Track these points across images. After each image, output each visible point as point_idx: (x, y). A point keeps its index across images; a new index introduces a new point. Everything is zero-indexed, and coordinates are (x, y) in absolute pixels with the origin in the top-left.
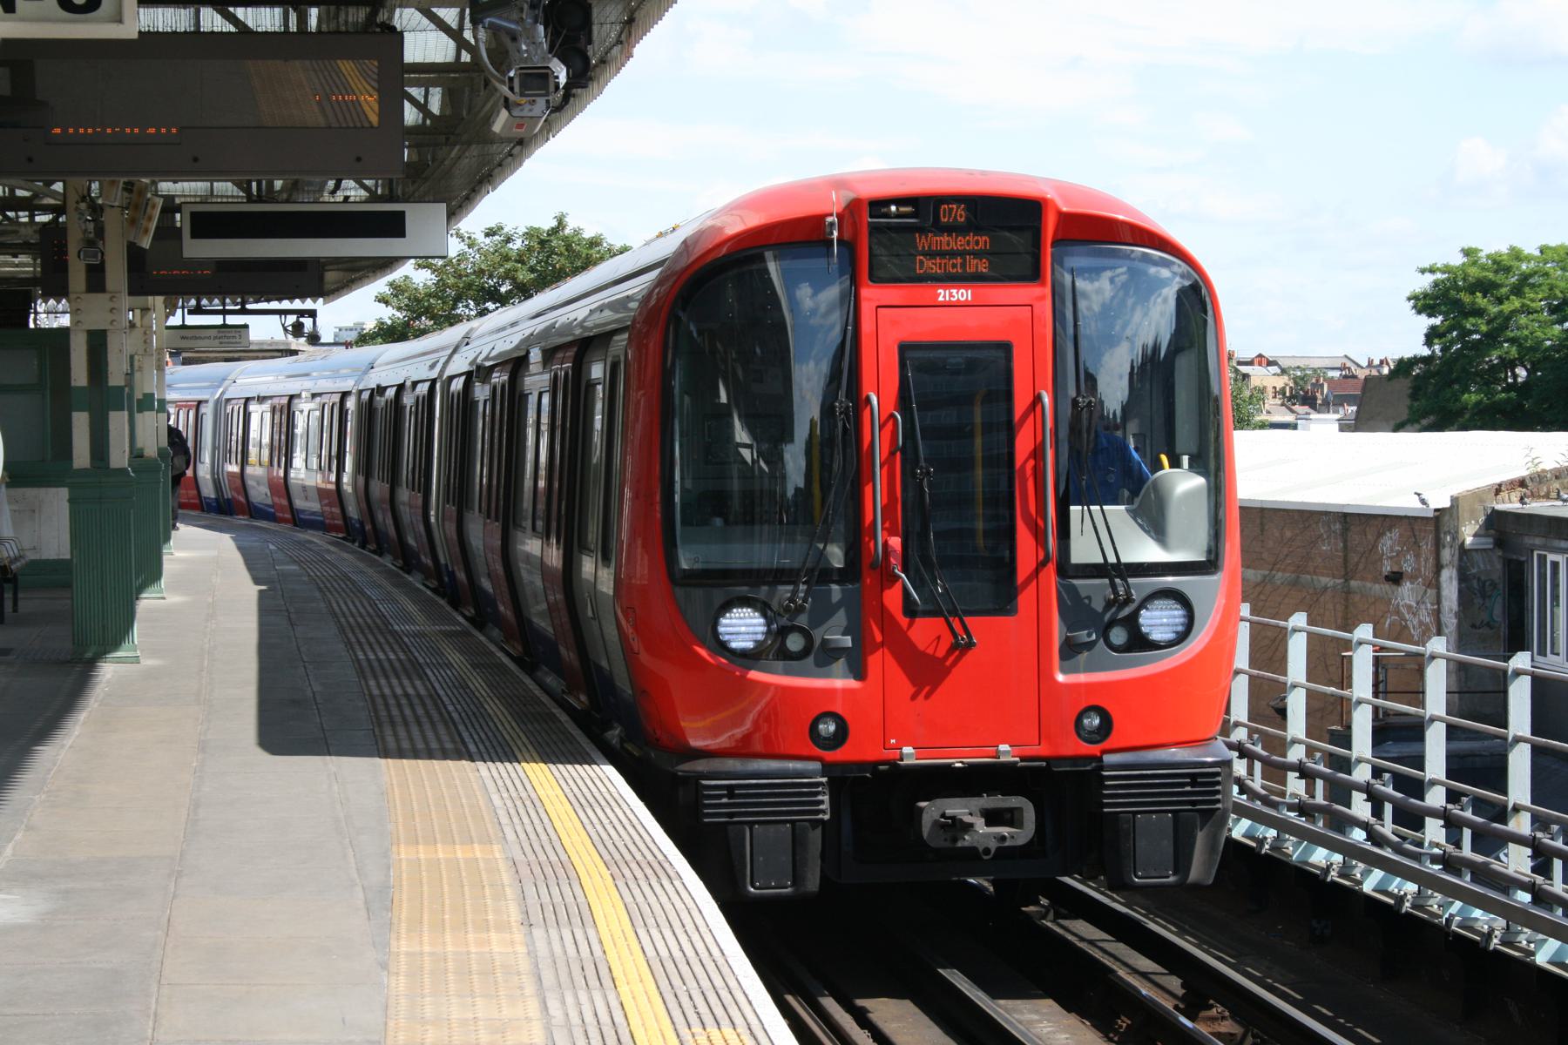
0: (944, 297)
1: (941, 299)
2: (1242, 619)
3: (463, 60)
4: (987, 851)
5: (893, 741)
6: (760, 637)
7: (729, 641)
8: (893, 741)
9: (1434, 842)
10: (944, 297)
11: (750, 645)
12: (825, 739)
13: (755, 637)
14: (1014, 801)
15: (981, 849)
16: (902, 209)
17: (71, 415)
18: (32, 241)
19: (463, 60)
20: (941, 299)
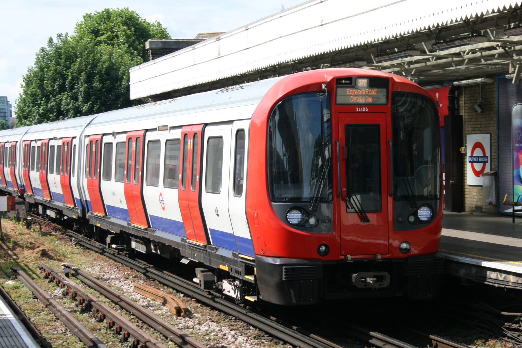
0: (358, 110)
1: (357, 110)
2: (514, 221)
3: (243, 306)
4: (375, 289)
5: (344, 253)
6: (300, 220)
7: (290, 221)
8: (344, 253)
9: (86, 136)
10: (358, 110)
11: (297, 222)
12: (323, 252)
13: (298, 220)
14: (383, 273)
15: (373, 288)
16: (346, 81)
17: (441, 229)
18: (288, 220)
19: (243, 306)
20: (357, 110)
